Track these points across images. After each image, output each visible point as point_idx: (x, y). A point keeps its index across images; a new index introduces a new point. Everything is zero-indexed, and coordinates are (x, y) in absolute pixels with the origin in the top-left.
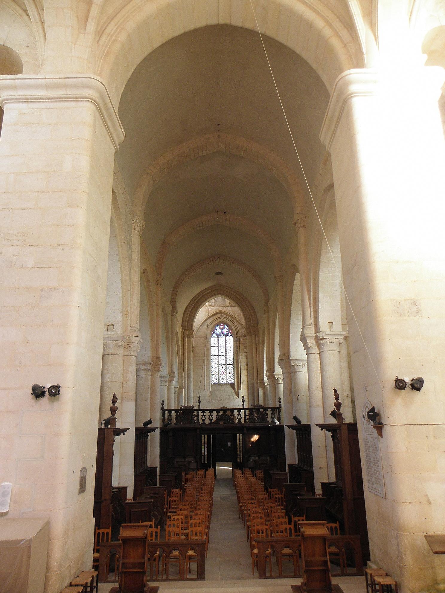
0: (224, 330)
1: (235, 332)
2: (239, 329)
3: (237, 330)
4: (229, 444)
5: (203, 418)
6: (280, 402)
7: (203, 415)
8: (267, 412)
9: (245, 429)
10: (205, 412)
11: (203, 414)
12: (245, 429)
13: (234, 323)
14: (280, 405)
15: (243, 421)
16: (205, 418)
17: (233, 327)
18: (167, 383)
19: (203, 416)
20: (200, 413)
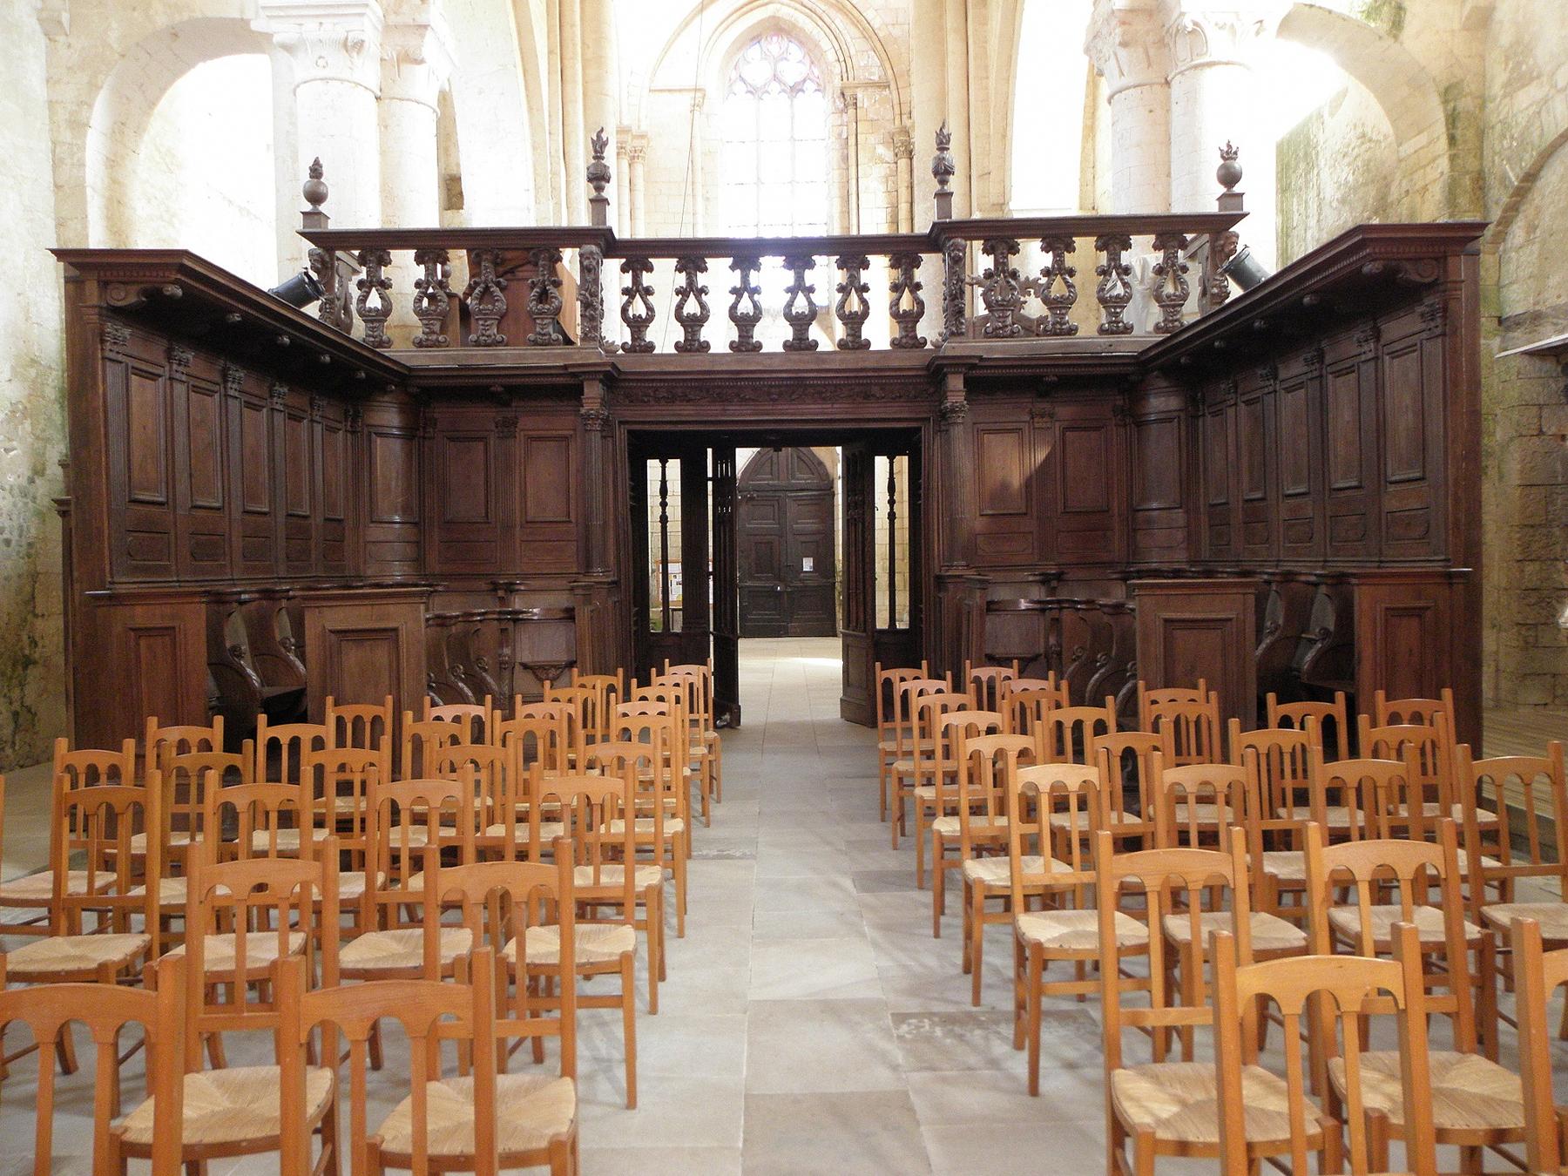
0: (782, 66)
1: (837, 70)
2: (853, 52)
3: (844, 60)
4: (808, 564)
5: (638, 308)
6: (1229, 178)
7: (637, 290)
8: (1123, 253)
9: (956, 383)
10: (650, 269)
11: (636, 280)
12: (956, 383)
13: (833, 27)
14: (1231, 198)
15: (929, 329)
16: (650, 309)
17: (825, 44)
18: (368, 71)
19: (633, 297)
20: (613, 274)
